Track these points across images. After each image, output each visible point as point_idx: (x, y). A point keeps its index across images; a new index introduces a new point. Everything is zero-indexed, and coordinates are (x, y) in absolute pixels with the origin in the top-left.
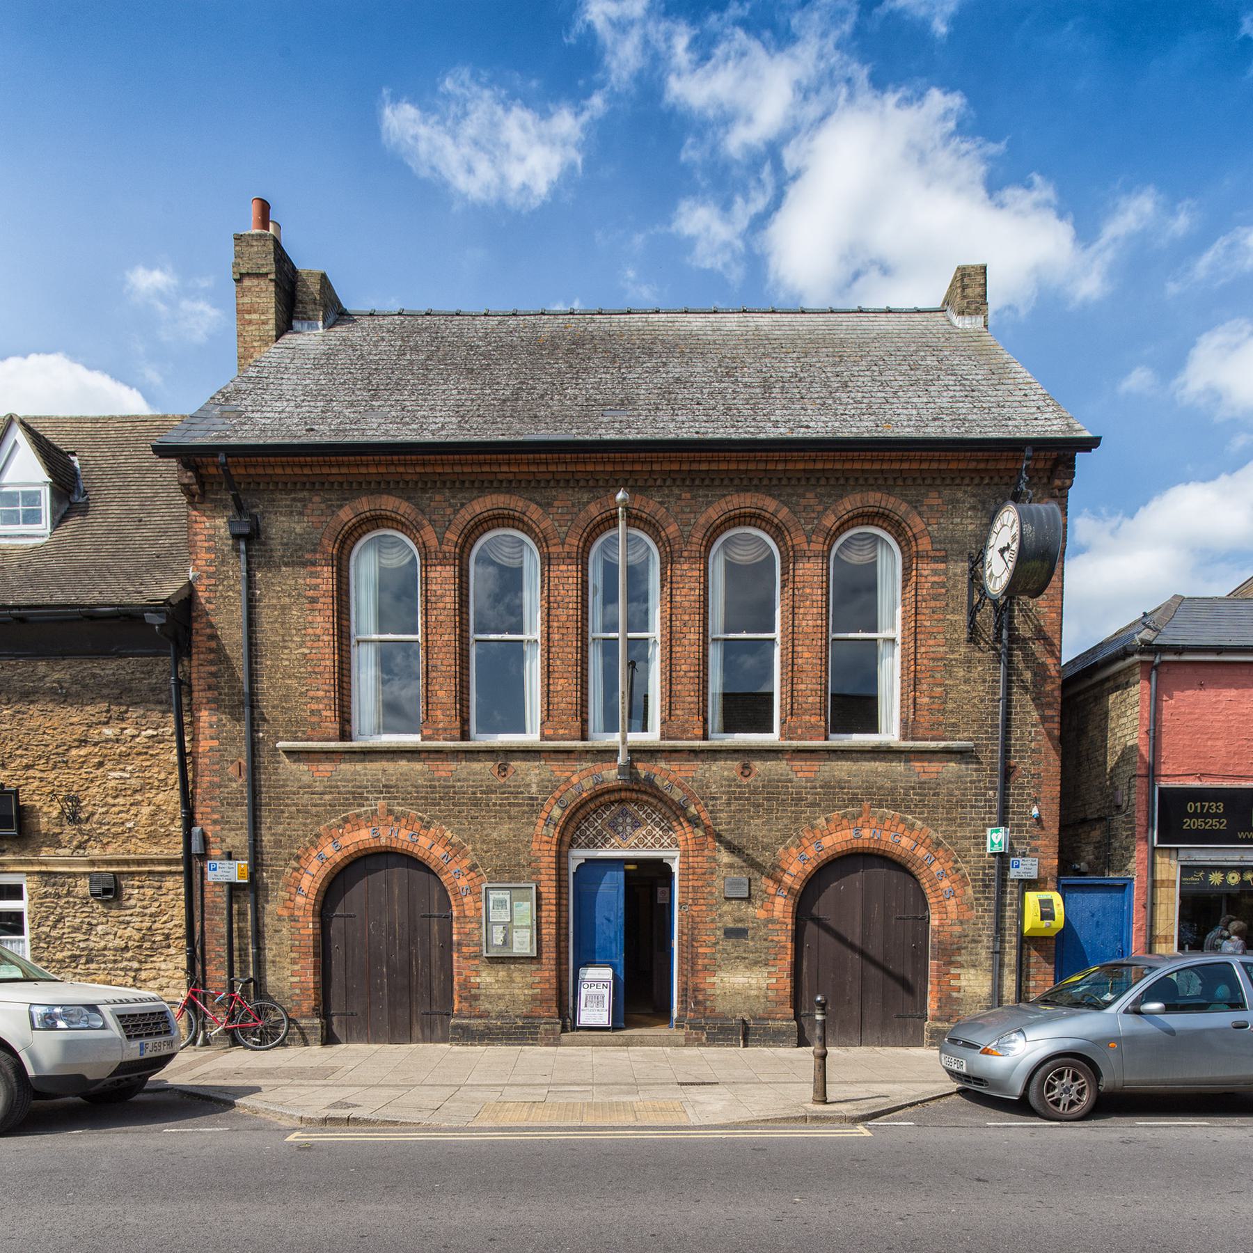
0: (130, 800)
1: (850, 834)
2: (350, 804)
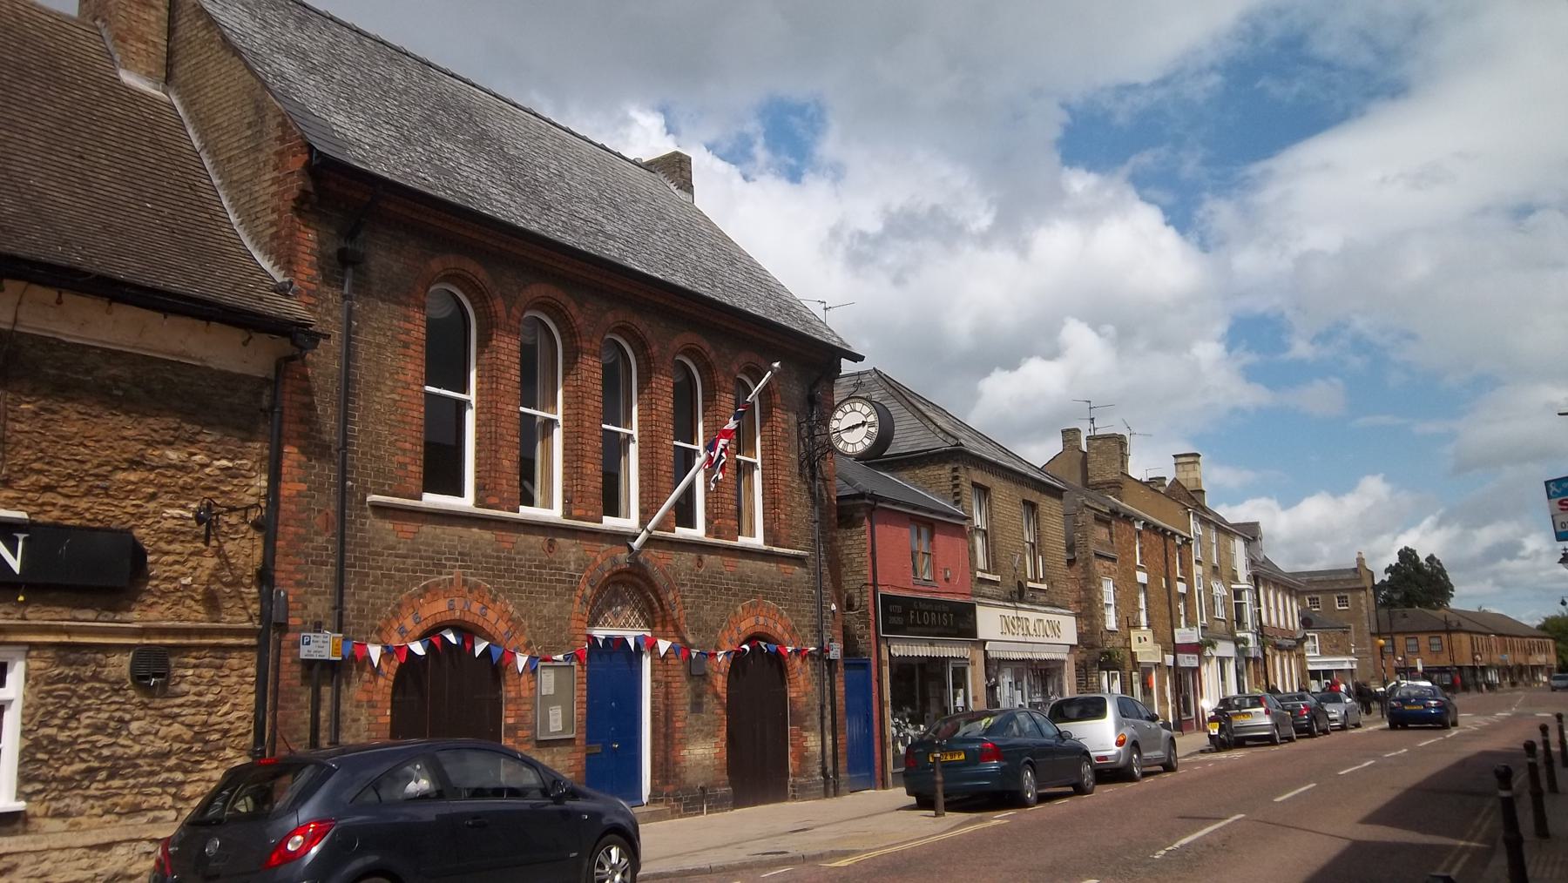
0: (190, 547)
2: (431, 572)
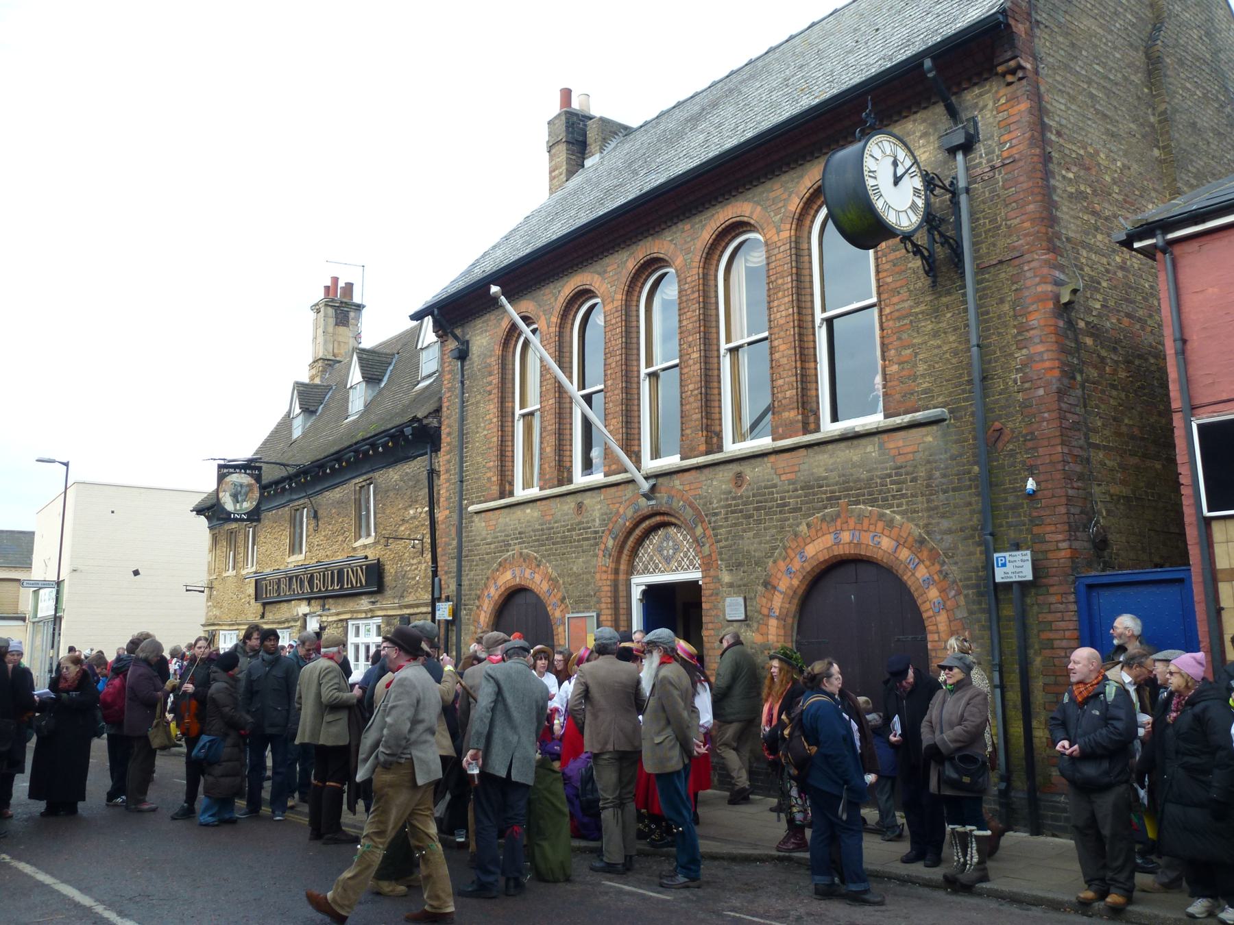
1: (828, 540)
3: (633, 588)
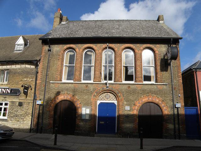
1: (147, 99)
3: (98, 103)
